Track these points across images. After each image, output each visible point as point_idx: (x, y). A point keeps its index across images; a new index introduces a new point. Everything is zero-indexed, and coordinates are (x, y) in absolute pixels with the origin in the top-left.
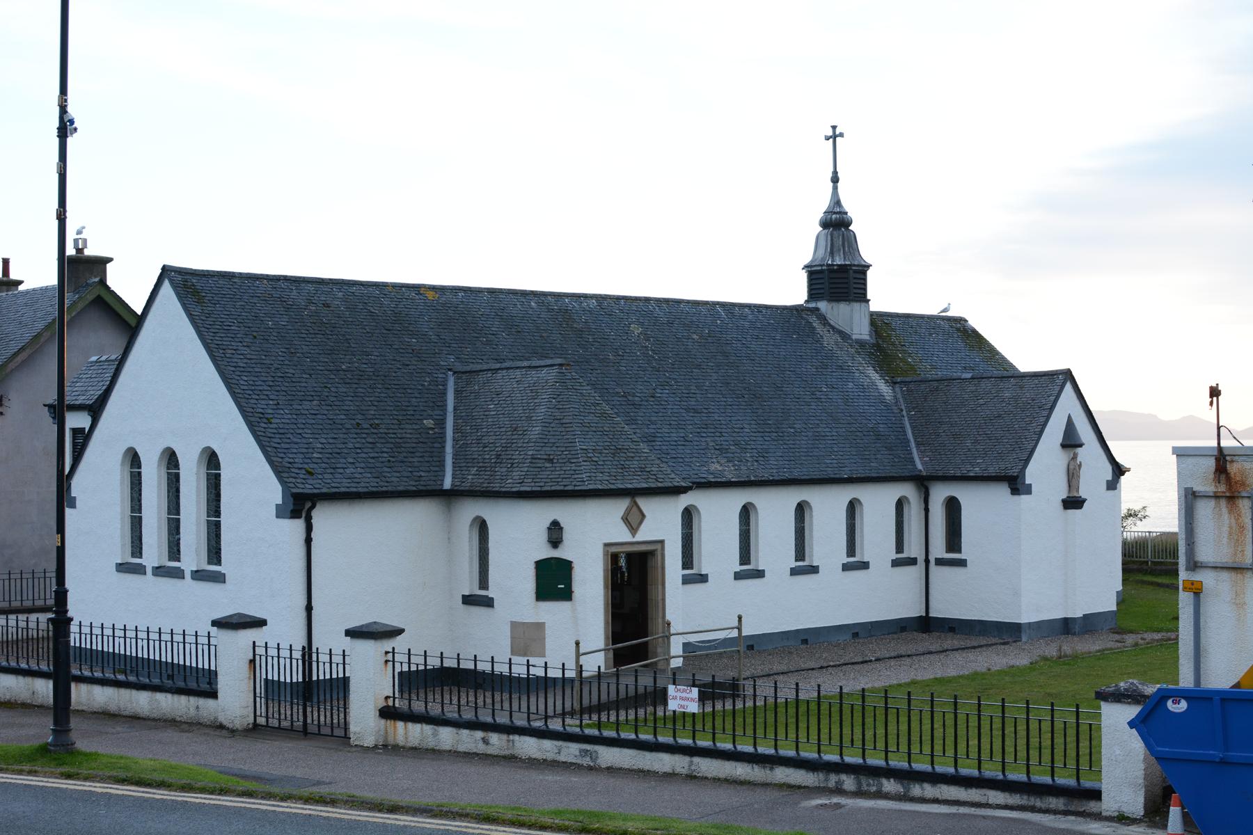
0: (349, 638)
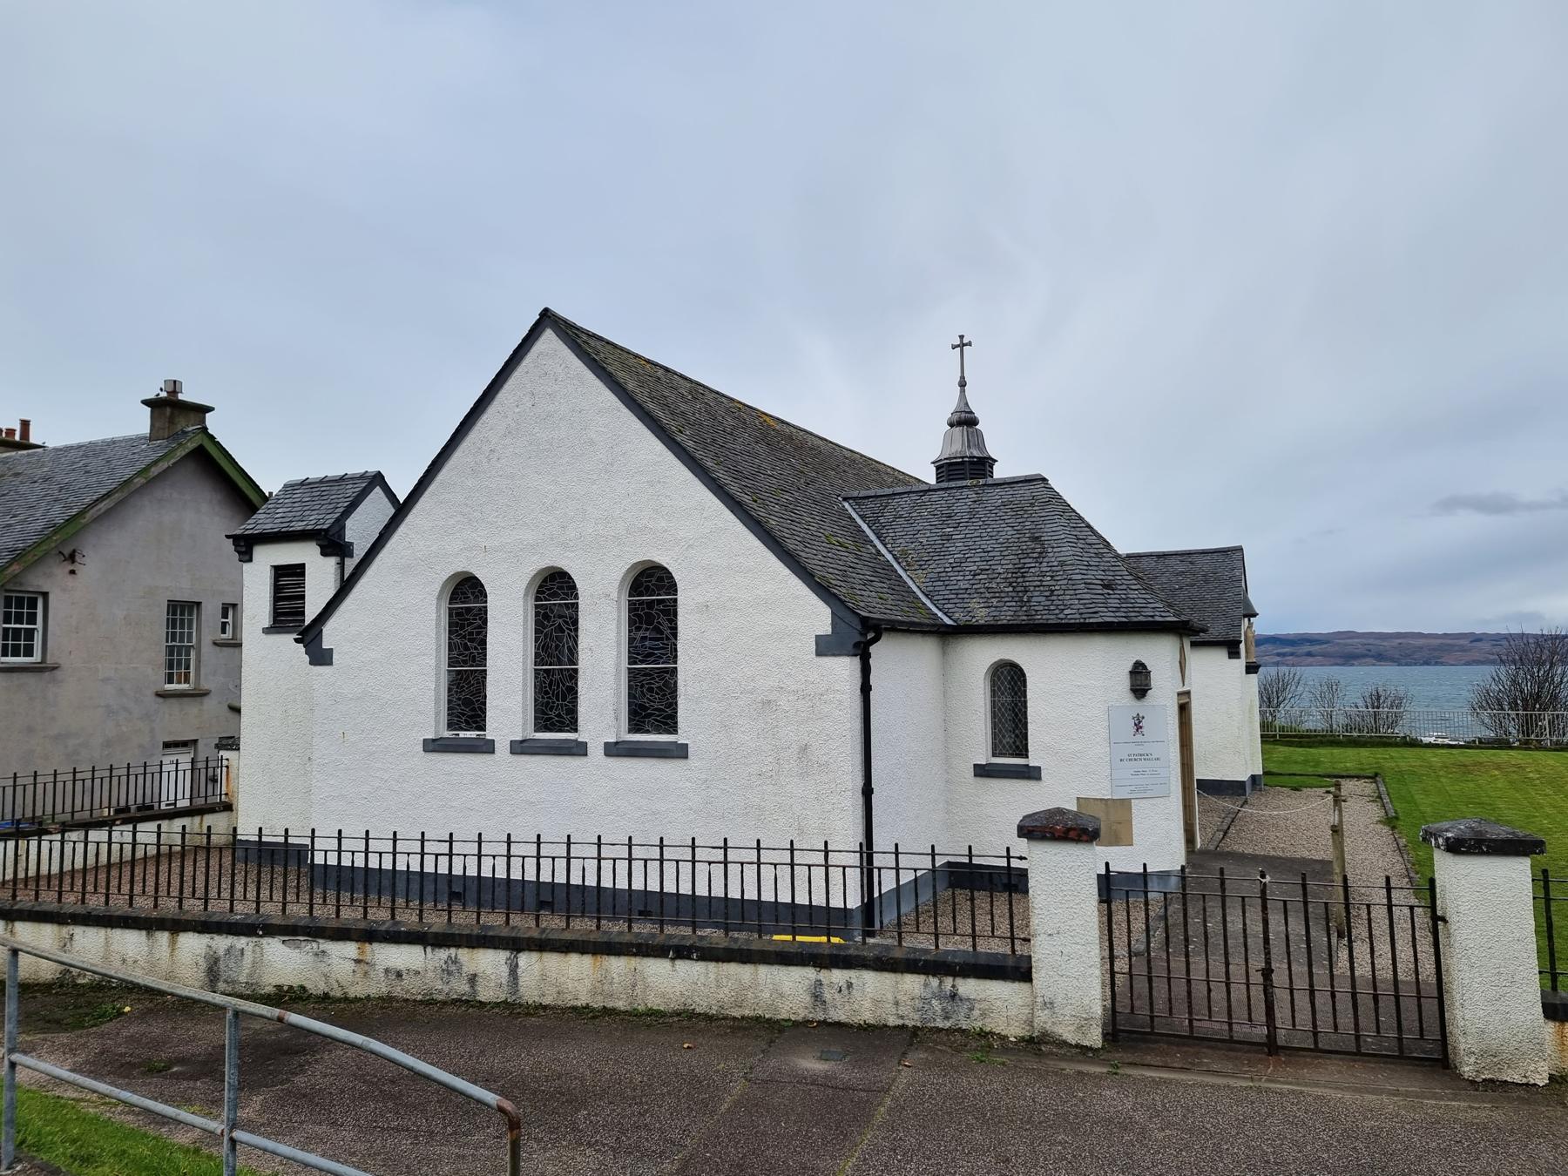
0: (1026, 840)
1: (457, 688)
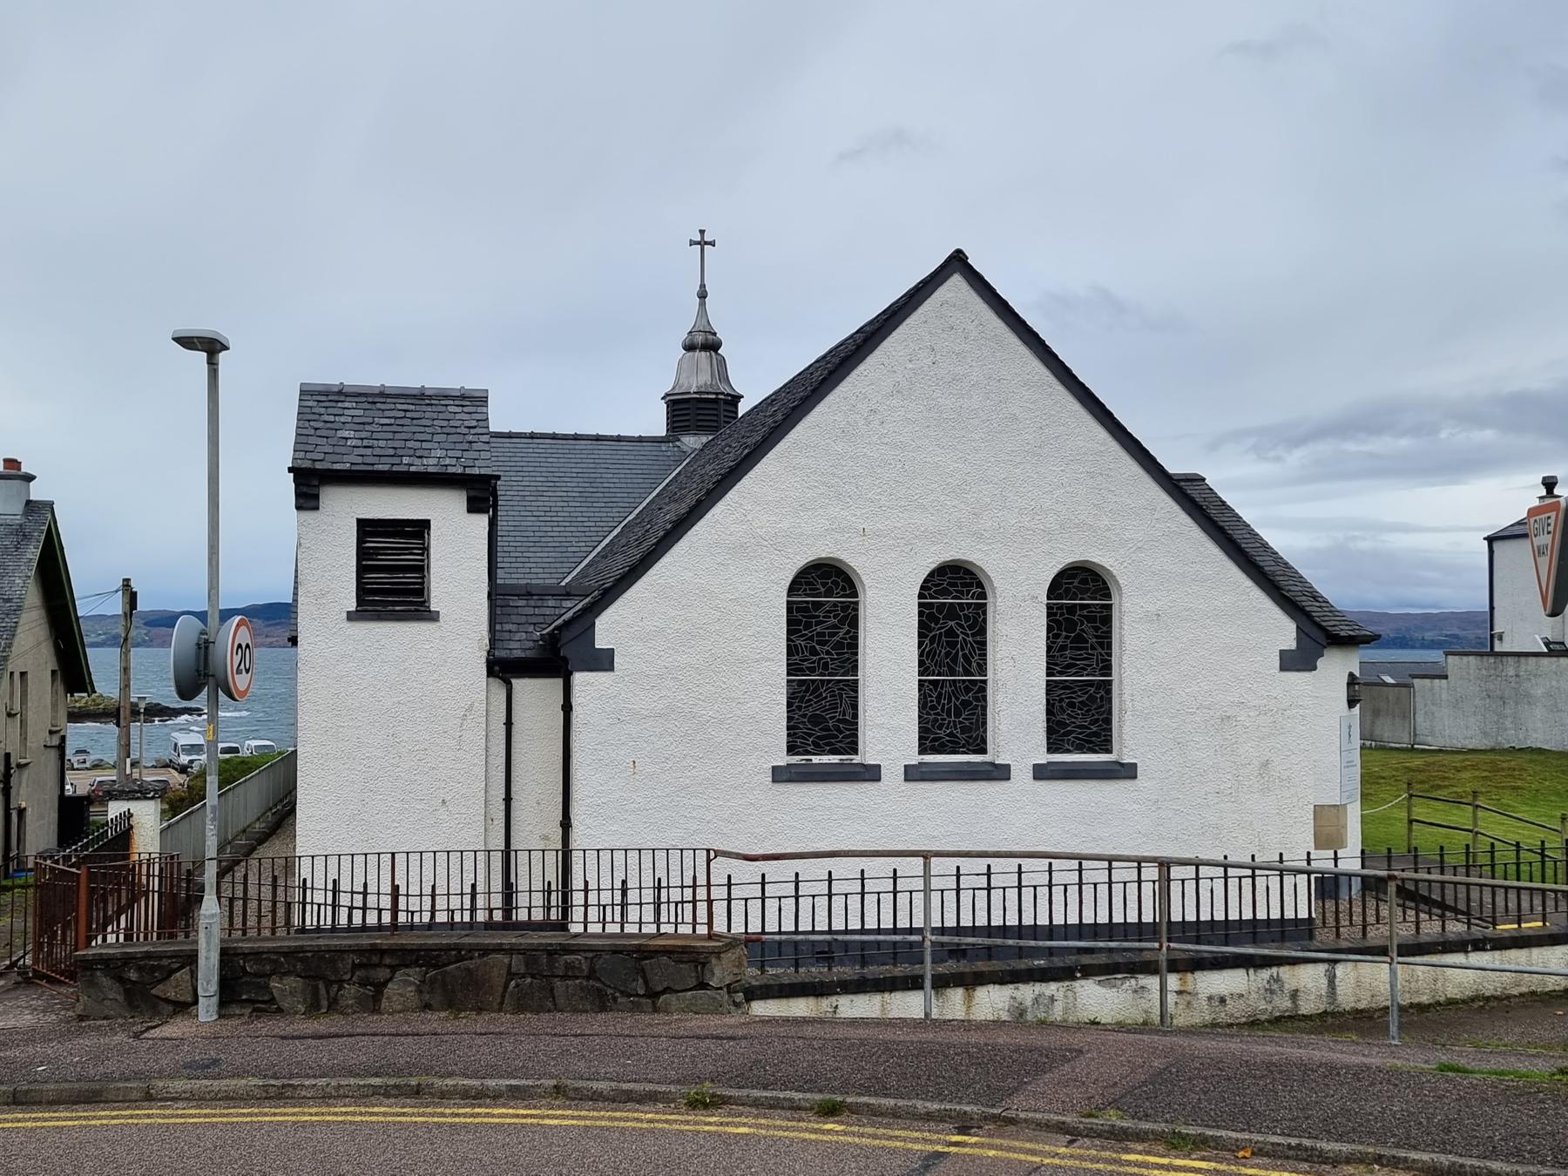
1: (801, 701)
